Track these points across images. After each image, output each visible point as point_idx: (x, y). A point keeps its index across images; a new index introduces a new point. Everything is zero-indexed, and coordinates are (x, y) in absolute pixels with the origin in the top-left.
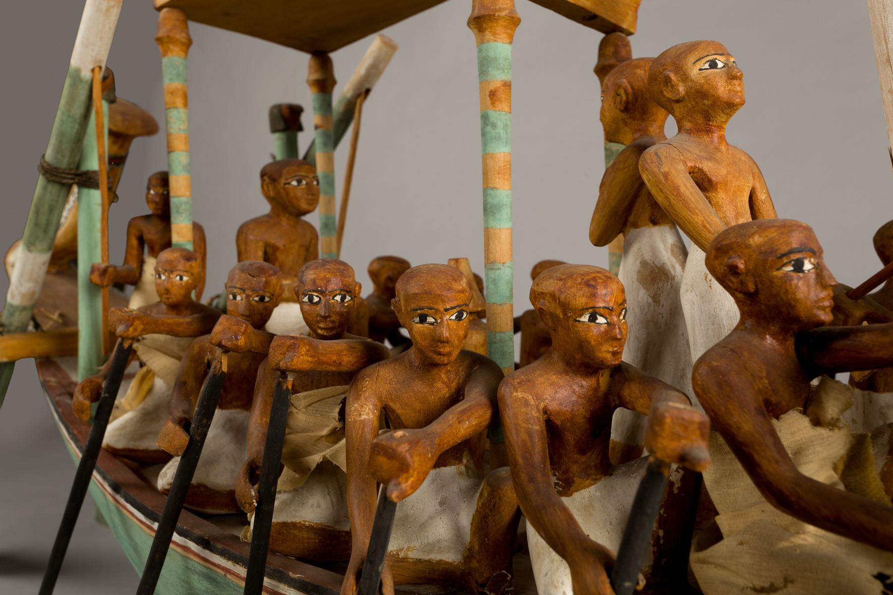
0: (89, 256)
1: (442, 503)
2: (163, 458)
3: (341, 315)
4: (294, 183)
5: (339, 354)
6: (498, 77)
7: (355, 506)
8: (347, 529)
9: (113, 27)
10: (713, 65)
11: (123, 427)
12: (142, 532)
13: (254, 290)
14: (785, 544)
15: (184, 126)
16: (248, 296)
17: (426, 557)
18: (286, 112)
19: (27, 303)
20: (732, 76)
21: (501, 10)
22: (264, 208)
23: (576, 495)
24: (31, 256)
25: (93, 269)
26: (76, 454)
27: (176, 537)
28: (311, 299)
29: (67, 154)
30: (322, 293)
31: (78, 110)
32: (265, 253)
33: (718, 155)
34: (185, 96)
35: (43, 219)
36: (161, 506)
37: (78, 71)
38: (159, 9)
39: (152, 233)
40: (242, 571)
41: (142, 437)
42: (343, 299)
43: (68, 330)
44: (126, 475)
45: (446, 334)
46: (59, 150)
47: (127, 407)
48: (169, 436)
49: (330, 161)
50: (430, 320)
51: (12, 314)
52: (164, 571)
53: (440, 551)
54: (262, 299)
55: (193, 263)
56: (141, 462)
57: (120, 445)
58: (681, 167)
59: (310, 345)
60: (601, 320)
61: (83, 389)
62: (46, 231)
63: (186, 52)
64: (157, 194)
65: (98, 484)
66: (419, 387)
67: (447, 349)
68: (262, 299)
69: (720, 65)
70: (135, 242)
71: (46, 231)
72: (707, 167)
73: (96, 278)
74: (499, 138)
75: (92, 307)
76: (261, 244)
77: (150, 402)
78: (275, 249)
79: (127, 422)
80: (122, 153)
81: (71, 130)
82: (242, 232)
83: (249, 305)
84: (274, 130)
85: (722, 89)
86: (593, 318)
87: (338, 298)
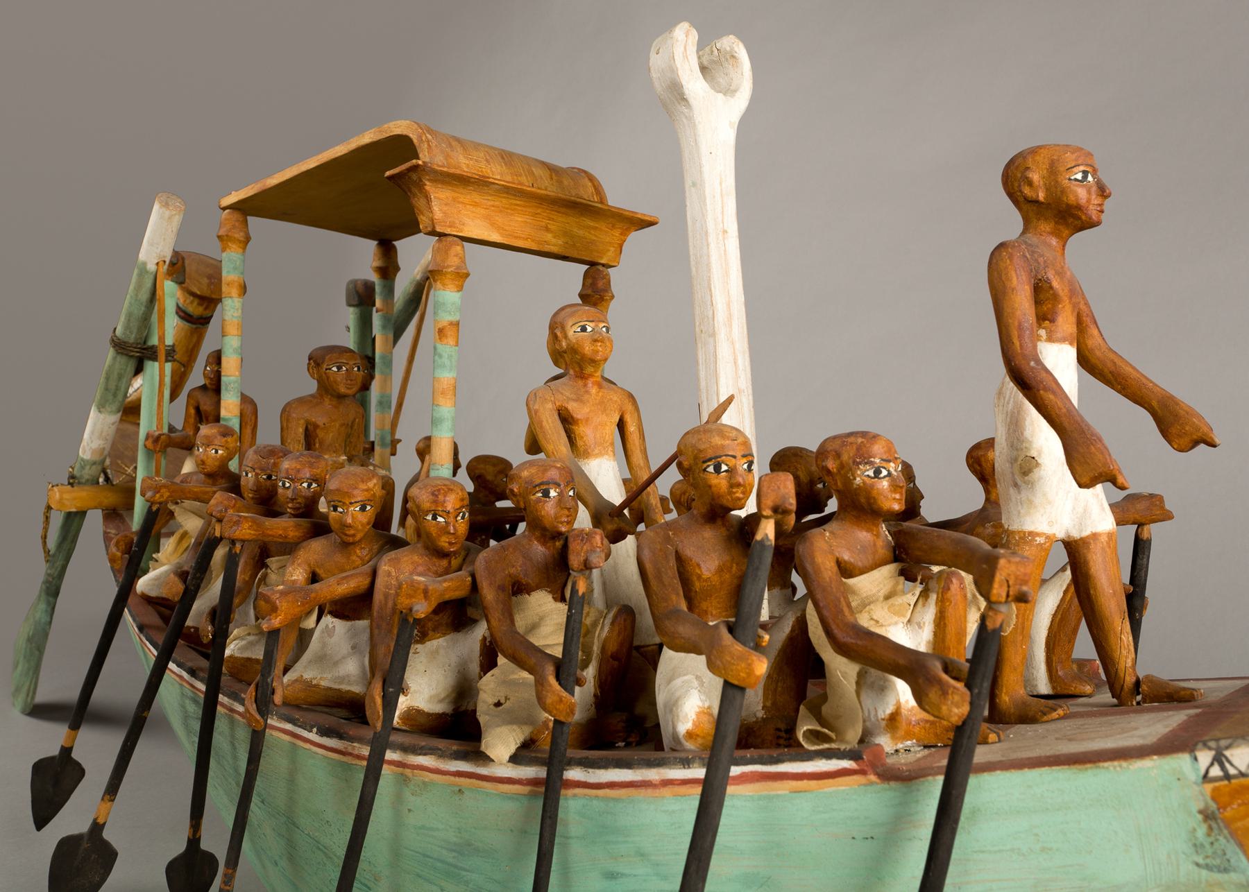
0: (147, 424)
1: (353, 648)
3: (306, 498)
4: (335, 369)
5: (285, 529)
8: (470, 708)
9: (175, 230)
10: (584, 329)
11: (157, 578)
13: (262, 470)
14: (516, 676)
16: (257, 474)
17: (336, 686)
18: (360, 288)
19: (97, 458)
20: (1103, 192)
21: (448, 266)
22: (311, 386)
23: (428, 643)
24: (102, 416)
27: (171, 665)
28: (284, 484)
29: (135, 331)
30: (292, 480)
31: (144, 296)
32: (306, 430)
33: (586, 397)
35: (112, 386)
37: (144, 264)
38: (224, 209)
39: (206, 406)
40: (203, 687)
42: (309, 486)
44: (153, 618)
45: (349, 521)
47: (164, 561)
50: (340, 509)
51: (83, 468)
53: (349, 683)
54: (269, 477)
55: (229, 439)
57: (153, 594)
58: (550, 406)
59: (254, 521)
60: (440, 519)
61: (117, 543)
62: (115, 395)
63: (244, 249)
64: (212, 371)
67: (352, 532)
68: (269, 477)
69: (589, 329)
70: (192, 411)
71: (115, 395)
72: (572, 407)
74: (444, 366)
75: (147, 468)
76: (302, 422)
78: (316, 426)
79: (162, 574)
80: (207, 314)
81: (139, 311)
82: (286, 412)
83: (257, 481)
84: (350, 305)
85: (588, 349)
86: (434, 518)
87: (305, 485)
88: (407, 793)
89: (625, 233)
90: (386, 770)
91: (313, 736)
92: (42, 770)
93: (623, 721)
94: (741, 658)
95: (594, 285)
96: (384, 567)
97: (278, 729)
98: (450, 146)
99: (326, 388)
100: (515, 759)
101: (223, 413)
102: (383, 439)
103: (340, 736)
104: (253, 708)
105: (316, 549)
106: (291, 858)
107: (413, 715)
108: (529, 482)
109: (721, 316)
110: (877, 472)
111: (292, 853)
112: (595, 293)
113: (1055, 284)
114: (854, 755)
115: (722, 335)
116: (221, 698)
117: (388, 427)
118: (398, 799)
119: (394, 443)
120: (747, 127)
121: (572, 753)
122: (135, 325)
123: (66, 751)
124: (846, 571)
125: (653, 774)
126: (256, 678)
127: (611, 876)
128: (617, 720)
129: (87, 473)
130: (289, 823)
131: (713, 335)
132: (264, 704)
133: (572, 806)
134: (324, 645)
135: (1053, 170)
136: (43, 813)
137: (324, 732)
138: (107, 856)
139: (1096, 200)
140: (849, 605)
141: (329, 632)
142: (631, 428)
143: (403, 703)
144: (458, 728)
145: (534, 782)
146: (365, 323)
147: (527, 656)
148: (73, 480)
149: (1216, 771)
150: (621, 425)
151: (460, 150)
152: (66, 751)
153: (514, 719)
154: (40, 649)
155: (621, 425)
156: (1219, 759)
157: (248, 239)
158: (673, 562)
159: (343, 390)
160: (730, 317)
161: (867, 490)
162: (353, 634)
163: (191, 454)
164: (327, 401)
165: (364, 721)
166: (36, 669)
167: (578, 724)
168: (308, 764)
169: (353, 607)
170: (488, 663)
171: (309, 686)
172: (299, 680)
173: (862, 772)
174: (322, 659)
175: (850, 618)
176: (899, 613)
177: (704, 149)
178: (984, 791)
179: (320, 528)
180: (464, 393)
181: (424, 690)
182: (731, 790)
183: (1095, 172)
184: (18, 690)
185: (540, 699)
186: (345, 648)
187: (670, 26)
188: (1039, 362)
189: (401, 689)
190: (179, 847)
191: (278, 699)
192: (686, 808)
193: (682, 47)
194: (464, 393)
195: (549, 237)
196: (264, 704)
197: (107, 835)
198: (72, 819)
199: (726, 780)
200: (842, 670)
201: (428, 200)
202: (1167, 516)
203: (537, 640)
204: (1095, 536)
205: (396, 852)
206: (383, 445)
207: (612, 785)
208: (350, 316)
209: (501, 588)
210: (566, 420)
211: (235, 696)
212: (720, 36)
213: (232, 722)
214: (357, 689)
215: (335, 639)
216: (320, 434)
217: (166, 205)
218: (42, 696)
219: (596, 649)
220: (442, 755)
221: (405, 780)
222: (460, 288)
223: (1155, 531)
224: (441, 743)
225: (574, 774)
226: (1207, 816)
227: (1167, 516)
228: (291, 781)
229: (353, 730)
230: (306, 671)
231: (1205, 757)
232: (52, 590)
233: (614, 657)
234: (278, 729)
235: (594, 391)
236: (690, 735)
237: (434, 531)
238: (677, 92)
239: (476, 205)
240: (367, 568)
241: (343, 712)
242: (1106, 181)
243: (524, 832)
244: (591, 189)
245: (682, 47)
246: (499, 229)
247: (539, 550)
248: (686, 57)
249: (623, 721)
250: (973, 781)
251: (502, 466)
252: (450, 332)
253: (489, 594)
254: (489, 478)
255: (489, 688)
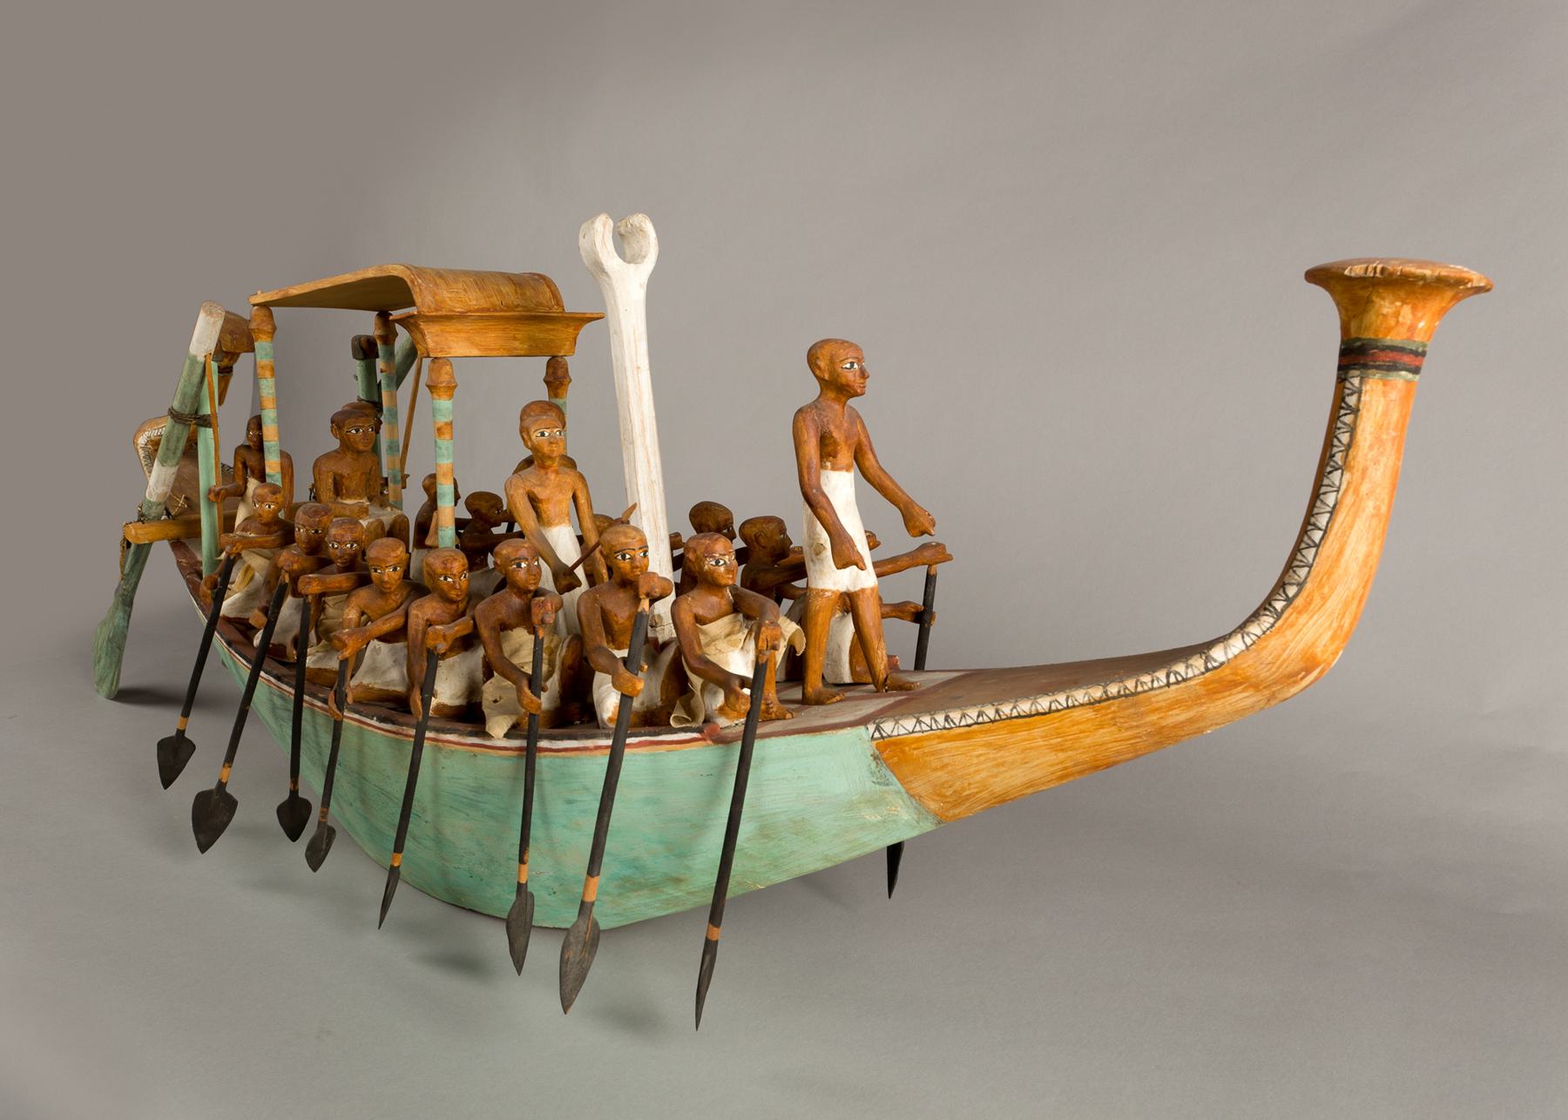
2: (256, 630)
6: (442, 420)
7: (1334, 603)
11: (233, 604)
12: (245, 669)
15: (272, 391)
18: (364, 345)
20: (863, 374)
22: (335, 444)
25: (210, 491)
26: (205, 621)
31: (196, 379)
34: (273, 369)
36: (253, 655)
39: (252, 461)
41: (246, 611)
43: (193, 517)
44: (237, 636)
46: (182, 403)
48: (256, 618)
49: (393, 398)
52: (256, 692)
56: (243, 628)
57: (232, 616)
65: (218, 640)
66: (380, 602)
73: (212, 497)
77: (252, 586)
81: (191, 391)
88: (441, 756)
89: (577, 329)
90: (426, 744)
91: (374, 722)
92: (163, 745)
93: (575, 711)
94: (629, 680)
95: (554, 373)
96: (413, 612)
97: (350, 718)
98: (436, 284)
99: (347, 446)
100: (507, 736)
101: (268, 471)
102: (394, 477)
103: (393, 723)
104: (334, 707)
105: (363, 595)
106: (363, 802)
107: (441, 708)
108: (507, 558)
109: (637, 429)
110: (717, 562)
111: (363, 798)
112: (556, 379)
113: (835, 435)
114: (699, 730)
115: (638, 442)
116: (306, 697)
117: (398, 466)
118: (435, 762)
119: (404, 478)
120: (656, 288)
121: (541, 731)
122: (188, 402)
123: (181, 733)
124: (700, 620)
125: (589, 743)
126: (334, 683)
127: (570, 802)
128: (574, 707)
129: (154, 512)
130: (361, 778)
131: (632, 443)
132: (341, 702)
133: (543, 762)
134: (374, 661)
135: (832, 362)
136: (168, 776)
137: (381, 720)
138: (231, 805)
139: (859, 380)
140: (699, 644)
141: (377, 651)
142: (582, 500)
143: (434, 702)
144: (470, 715)
145: (520, 749)
146: (370, 372)
147: (511, 672)
148: (142, 518)
149: (877, 735)
150: (575, 498)
151: (443, 286)
152: (181, 733)
153: (505, 711)
154: (121, 648)
155: (575, 498)
156: (878, 729)
157: (274, 329)
158: (598, 615)
159: (361, 447)
160: (644, 430)
161: (711, 573)
162: (394, 652)
163: (243, 500)
164: (349, 455)
165: (409, 712)
166: (119, 662)
167: (548, 711)
168: (373, 741)
169: (395, 635)
170: (488, 674)
171: (367, 689)
172: (360, 685)
173: (703, 739)
174: (373, 670)
175: (699, 652)
176: (734, 645)
177: (621, 308)
178: (760, 748)
179: (364, 581)
180: (457, 439)
181: (447, 691)
182: (627, 751)
183: (860, 361)
184: (101, 680)
185: (520, 701)
186: (389, 662)
187: (591, 216)
188: (819, 489)
189: (433, 694)
190: (286, 796)
191: (350, 700)
192: (603, 760)
193: (600, 232)
194: (457, 439)
195: (517, 344)
196: (341, 702)
197: (229, 790)
198: (197, 777)
199: (625, 745)
200: (696, 681)
201: (423, 335)
202: (948, 558)
203: (515, 661)
204: (863, 590)
205: (436, 795)
206: (395, 482)
207: (566, 750)
208: (357, 367)
209: (493, 628)
210: (534, 501)
211: (314, 696)
212: (633, 213)
213: (313, 712)
214: (400, 689)
215: (380, 657)
216: (346, 482)
217: (210, 314)
218: (125, 683)
219: (558, 663)
220: (461, 733)
221: (440, 749)
222: (451, 397)
223: (941, 570)
224: (461, 726)
225: (543, 744)
226: (875, 758)
227: (948, 558)
228: (360, 751)
229: (407, 719)
230: (362, 680)
231: (872, 727)
232: (126, 600)
233: (570, 667)
234: (350, 718)
235: (552, 476)
236: (610, 719)
237: (445, 588)
238: (599, 268)
239: (459, 331)
240: (401, 611)
241: (394, 706)
242: (869, 370)
243: (515, 778)
244: (549, 295)
245: (600, 232)
246: (477, 345)
247: (516, 601)
248: (604, 244)
249: (575, 711)
250: (758, 744)
251: (494, 500)
252: (446, 431)
253: (485, 633)
254: (484, 511)
255: (490, 690)
